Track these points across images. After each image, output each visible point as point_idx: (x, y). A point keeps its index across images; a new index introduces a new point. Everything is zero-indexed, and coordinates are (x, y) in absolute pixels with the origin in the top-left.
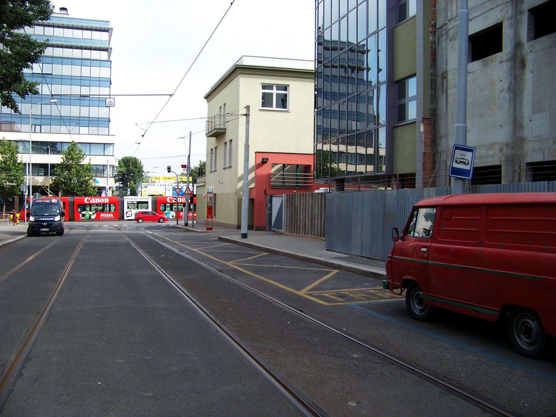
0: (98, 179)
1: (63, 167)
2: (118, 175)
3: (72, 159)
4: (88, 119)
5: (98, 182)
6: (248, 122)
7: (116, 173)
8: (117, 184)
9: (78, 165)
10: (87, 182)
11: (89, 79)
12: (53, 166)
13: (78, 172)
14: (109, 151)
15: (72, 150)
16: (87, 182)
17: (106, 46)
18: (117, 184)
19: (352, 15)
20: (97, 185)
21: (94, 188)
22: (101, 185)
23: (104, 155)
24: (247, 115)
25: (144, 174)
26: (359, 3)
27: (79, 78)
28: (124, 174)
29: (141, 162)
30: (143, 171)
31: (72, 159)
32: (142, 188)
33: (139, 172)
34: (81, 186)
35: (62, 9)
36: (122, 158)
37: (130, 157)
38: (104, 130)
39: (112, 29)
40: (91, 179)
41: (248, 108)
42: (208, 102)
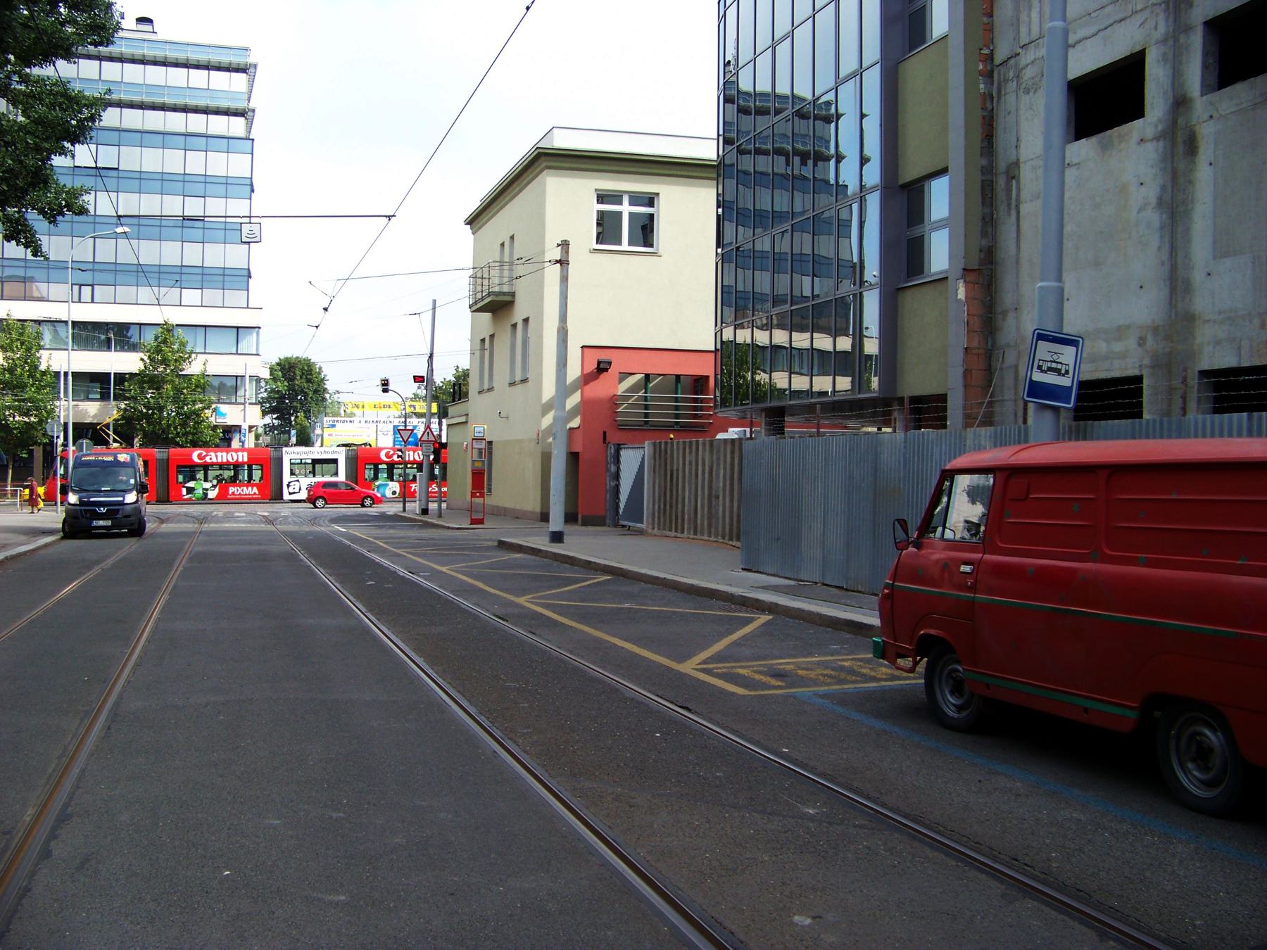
0: (223, 408)
1: (144, 379)
2: (268, 399)
3: (165, 362)
4: (199, 271)
5: (224, 415)
6: (564, 279)
7: (265, 395)
8: (268, 420)
9: (179, 376)
10: (197, 414)
11: (202, 179)
12: (121, 378)
13: (178, 391)
14: (248, 343)
15: (165, 341)
16: (197, 414)
17: (241, 105)
18: (268, 420)
19: (803, 34)
20: (220, 421)
21: (215, 428)
22: (230, 421)
23: (237, 354)
24: (563, 262)
25: (327, 396)
26: (817, 8)
27: (181, 178)
28: (282, 397)
29: (320, 368)
30: (325, 390)
31: (165, 362)
32: (322, 429)
33: (316, 391)
34: (184, 425)
35: (142, 20)
36: (277, 361)
37: (297, 358)
38: (238, 297)
39: (255, 66)
40: (208, 408)
41: (565, 245)
42: (473, 233)
